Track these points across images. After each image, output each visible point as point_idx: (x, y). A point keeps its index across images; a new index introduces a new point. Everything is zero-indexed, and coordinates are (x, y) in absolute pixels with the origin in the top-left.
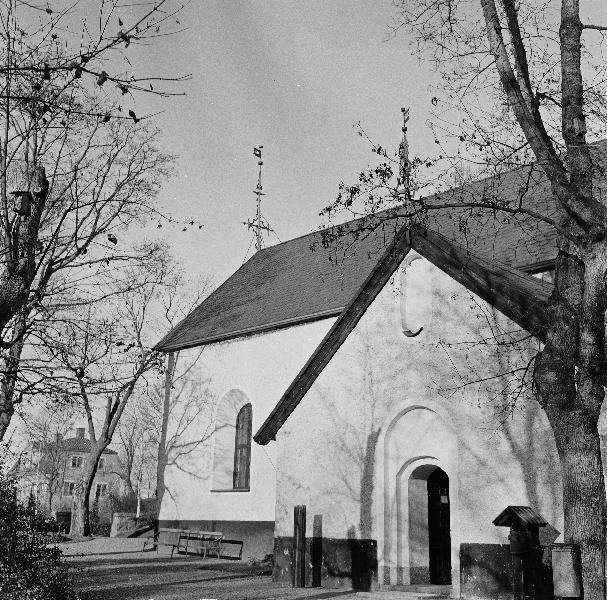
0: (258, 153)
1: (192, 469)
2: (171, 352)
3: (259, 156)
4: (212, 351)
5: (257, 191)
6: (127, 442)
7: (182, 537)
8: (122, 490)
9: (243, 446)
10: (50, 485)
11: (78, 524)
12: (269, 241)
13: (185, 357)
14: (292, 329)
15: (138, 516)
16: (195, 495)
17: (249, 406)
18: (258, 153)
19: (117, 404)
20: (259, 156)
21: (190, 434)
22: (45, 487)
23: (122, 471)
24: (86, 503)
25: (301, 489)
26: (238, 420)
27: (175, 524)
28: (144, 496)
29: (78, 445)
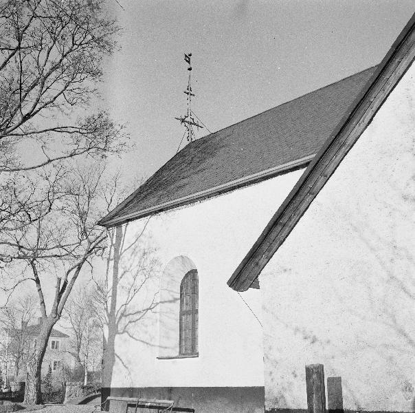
0: (188, 58)
1: (146, 338)
2: (118, 225)
3: (189, 62)
4: (153, 219)
5: (188, 91)
6: (76, 327)
7: (130, 405)
8: (72, 364)
9: (187, 313)
10: (17, 363)
11: (31, 394)
12: (199, 134)
13: (132, 229)
14: (236, 192)
15: (85, 384)
16: (144, 362)
17: (195, 271)
18: (188, 58)
19: (65, 284)
20: (189, 62)
21: (140, 301)
22: (14, 364)
23: (74, 351)
24: (38, 374)
25: (317, 343)
26: (181, 288)
27: (131, 391)
28: (90, 369)
29: (34, 331)
